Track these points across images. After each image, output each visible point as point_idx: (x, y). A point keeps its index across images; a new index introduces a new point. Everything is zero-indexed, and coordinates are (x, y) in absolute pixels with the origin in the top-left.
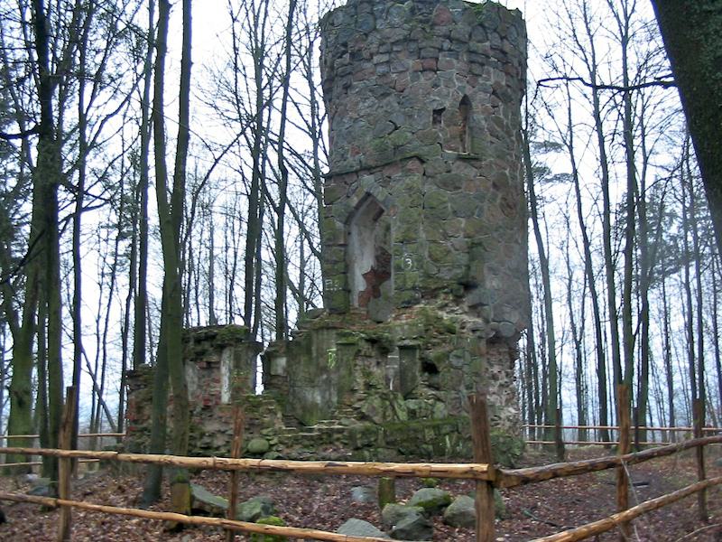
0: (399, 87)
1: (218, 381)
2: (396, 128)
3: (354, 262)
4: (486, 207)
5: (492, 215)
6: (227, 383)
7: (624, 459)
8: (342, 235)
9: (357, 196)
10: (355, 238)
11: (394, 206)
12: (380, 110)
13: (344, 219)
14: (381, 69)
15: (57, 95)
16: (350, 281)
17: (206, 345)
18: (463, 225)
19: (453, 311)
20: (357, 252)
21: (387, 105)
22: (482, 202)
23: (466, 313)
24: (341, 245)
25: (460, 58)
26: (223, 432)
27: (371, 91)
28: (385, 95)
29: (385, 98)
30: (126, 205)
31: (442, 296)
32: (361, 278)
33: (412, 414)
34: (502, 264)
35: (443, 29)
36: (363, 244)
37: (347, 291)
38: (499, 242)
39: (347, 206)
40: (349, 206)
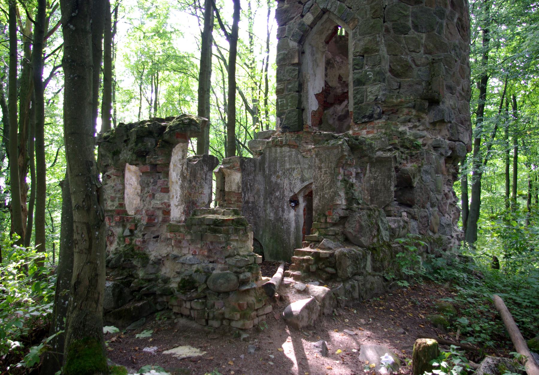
1: (166, 190)
3: (308, 81)
4: (445, 24)
5: (451, 33)
6: (179, 193)
8: (297, 54)
9: (312, 14)
10: (308, 58)
13: (299, 38)
16: (304, 99)
17: (150, 143)
18: (423, 41)
19: (415, 127)
20: (311, 72)
22: (441, 19)
23: (427, 129)
24: (293, 65)
26: (176, 258)
31: (406, 111)
32: (314, 98)
33: (393, 233)
34: (458, 84)
36: (315, 63)
37: (301, 110)
38: (456, 61)
39: (302, 24)
40: (303, 25)
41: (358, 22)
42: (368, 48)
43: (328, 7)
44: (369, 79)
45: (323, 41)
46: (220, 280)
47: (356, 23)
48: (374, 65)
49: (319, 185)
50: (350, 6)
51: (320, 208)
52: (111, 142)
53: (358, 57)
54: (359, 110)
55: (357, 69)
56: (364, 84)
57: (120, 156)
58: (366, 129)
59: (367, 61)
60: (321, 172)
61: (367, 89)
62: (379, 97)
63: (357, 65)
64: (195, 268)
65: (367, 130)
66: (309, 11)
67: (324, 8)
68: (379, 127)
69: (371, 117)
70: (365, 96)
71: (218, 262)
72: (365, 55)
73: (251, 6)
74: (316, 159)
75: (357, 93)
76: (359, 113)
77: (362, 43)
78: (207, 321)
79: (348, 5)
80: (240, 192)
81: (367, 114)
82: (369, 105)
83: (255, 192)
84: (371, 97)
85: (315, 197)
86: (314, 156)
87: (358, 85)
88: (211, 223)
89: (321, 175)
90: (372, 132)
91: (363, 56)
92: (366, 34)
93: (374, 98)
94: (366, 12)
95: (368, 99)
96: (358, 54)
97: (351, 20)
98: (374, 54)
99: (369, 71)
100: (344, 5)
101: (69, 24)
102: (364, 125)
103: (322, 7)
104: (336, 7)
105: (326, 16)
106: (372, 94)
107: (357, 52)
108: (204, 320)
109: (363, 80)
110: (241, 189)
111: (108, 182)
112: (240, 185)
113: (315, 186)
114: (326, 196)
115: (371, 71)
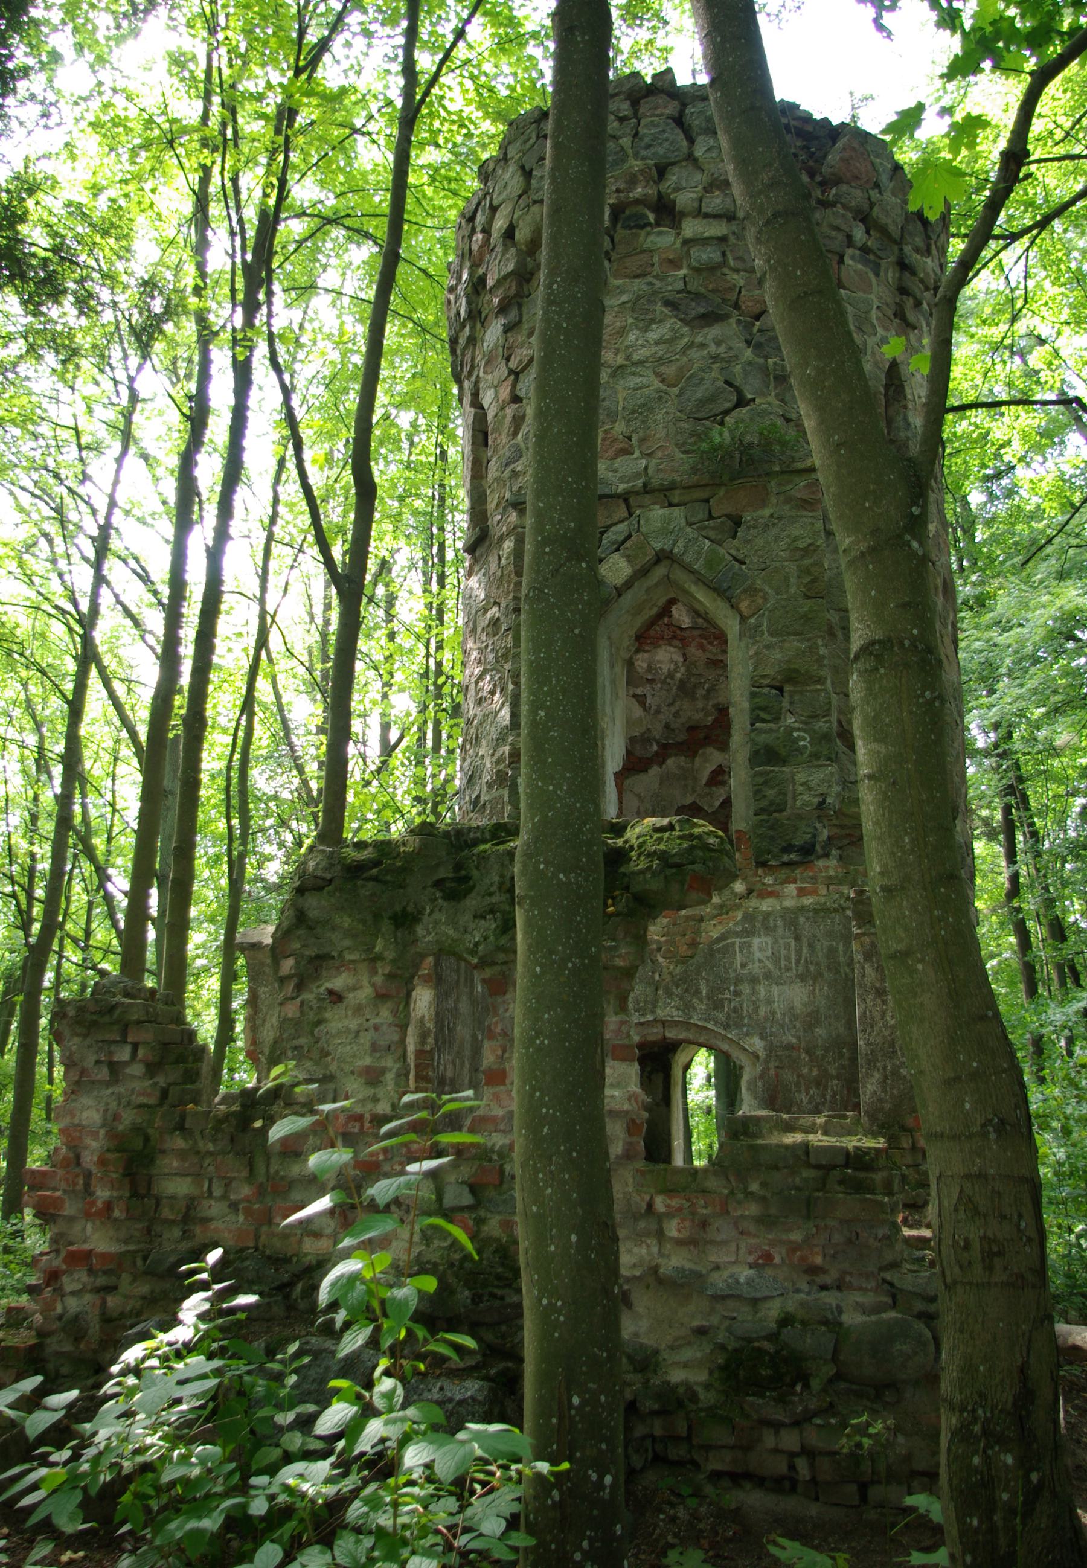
0: (746, 305)
2: (741, 402)
7: (511, 854)
9: (629, 558)
11: (752, 591)
12: (694, 354)
14: (708, 255)
15: (697, 1121)
21: (718, 343)
25: (882, 274)
27: (667, 303)
28: (709, 318)
29: (710, 325)
30: (272, 804)
35: (856, 196)
41: (765, 599)
42: (797, 671)
43: (676, 550)
44: (800, 751)
45: (632, 633)
46: (898, 1346)
47: (760, 601)
48: (815, 717)
49: (879, 1040)
50: (740, 557)
51: (887, 1106)
52: (385, 883)
53: (766, 690)
54: (771, 828)
55: (763, 721)
56: (784, 762)
57: (420, 930)
58: (795, 882)
59: (791, 703)
60: (884, 1002)
61: (793, 774)
62: (829, 800)
63: (763, 709)
64: (773, 1311)
65: (799, 885)
66: (617, 550)
67: (662, 550)
68: (829, 881)
69: (808, 851)
70: (790, 795)
71: (850, 1287)
72: (787, 688)
73: (271, 495)
74: (867, 966)
75: (765, 783)
76: (772, 838)
77: (777, 655)
78: (863, 1488)
79: (733, 552)
80: (428, 1048)
81: (798, 842)
82: (800, 817)
83: (455, 1048)
84: (806, 798)
85: (869, 1075)
86: (858, 957)
87: (768, 762)
88: (841, 1160)
89: (884, 1013)
90: (814, 892)
91: (781, 690)
92: (789, 634)
93: (816, 800)
94: (787, 579)
95: (798, 803)
96: (766, 682)
97: (745, 591)
98: (813, 687)
99: (798, 730)
100: (722, 551)
101: (908, 537)
102: (784, 872)
103: (658, 546)
104: (699, 553)
105: (660, 571)
106: (810, 789)
107: (764, 677)
108: (853, 1488)
109: (783, 752)
110: (430, 1040)
111: (328, 1015)
112: (430, 1025)
113: (867, 1044)
114: (903, 1071)
115: (805, 731)
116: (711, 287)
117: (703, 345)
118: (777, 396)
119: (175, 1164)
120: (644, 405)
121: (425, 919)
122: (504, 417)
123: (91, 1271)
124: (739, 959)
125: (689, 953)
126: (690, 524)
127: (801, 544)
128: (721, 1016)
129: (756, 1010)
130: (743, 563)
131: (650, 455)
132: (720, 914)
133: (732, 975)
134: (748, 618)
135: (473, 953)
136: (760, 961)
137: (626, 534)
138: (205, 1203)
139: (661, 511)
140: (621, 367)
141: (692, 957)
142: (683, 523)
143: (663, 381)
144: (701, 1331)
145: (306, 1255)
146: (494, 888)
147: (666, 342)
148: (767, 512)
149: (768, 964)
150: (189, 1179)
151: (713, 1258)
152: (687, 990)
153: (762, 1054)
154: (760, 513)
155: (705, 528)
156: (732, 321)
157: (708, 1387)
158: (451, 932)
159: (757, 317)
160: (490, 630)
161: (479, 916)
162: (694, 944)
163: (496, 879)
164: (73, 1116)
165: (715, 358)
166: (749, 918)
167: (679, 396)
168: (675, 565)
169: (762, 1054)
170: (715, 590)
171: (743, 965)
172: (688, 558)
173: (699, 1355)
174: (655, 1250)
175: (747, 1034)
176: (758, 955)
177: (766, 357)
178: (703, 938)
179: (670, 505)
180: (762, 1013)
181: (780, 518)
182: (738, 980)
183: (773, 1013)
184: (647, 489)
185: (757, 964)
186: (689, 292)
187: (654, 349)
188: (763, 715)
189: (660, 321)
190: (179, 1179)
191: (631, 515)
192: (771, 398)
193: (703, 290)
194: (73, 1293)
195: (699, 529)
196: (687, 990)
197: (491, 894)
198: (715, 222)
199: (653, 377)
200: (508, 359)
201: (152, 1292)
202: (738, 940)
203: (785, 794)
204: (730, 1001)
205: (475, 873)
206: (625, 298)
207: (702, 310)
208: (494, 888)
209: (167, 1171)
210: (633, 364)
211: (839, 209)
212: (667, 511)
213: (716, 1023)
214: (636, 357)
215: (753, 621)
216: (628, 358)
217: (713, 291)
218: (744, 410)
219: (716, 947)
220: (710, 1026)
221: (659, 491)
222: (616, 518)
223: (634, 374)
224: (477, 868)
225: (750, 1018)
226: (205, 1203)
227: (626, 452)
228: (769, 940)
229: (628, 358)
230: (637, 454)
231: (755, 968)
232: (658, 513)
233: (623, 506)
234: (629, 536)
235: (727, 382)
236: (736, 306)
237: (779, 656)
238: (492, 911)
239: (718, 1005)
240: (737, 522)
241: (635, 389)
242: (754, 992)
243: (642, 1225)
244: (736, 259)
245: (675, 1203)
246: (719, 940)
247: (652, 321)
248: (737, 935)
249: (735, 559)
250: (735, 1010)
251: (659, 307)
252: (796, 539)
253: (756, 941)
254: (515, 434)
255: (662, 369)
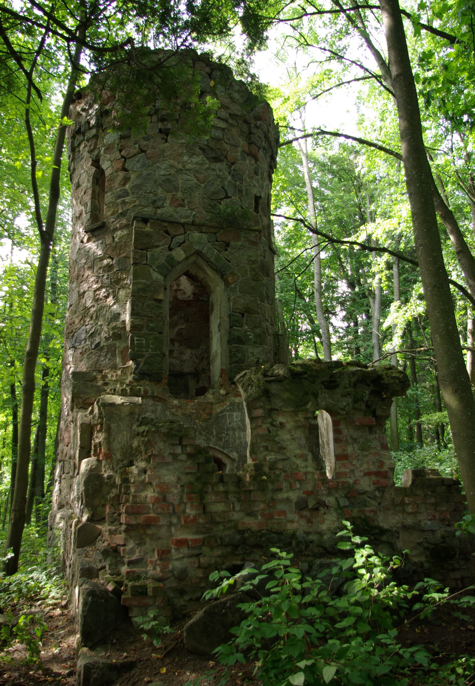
2: (227, 197)
9: (184, 251)
11: (233, 274)
27: (201, 148)
28: (216, 159)
41: (238, 278)
43: (203, 251)
44: (250, 340)
48: (255, 327)
50: (229, 259)
53: (237, 314)
55: (236, 326)
56: (244, 343)
64: (439, 534)
66: (179, 246)
72: (245, 314)
79: (226, 256)
84: (252, 358)
88: (452, 483)
91: (243, 315)
93: (256, 360)
95: (249, 360)
96: (238, 311)
97: (230, 273)
99: (249, 331)
106: (254, 355)
107: (237, 309)
116: (218, 147)
117: (214, 170)
118: (239, 197)
119: (213, 498)
120: (190, 188)
121: (320, 395)
122: (118, 176)
123: (188, 547)
124: (228, 421)
125: (208, 417)
126: (209, 242)
127: (252, 259)
128: (222, 444)
129: (235, 441)
130: (229, 262)
131: (192, 209)
132: (219, 403)
133: (225, 427)
134: (230, 284)
135: (343, 409)
136: (236, 422)
137: (183, 240)
138: (230, 514)
139: (198, 234)
140: (181, 169)
141: (210, 419)
142: (207, 241)
143: (198, 180)
144: (419, 544)
145: (288, 530)
146: (347, 386)
147: (199, 164)
148: (240, 243)
149: (240, 423)
150: (223, 504)
151: (419, 518)
152: (208, 433)
153: (237, 459)
154: (237, 243)
155: (215, 244)
156: (225, 163)
157: (426, 562)
158: (331, 401)
159: (233, 164)
160: (106, 269)
161: (344, 396)
162: (210, 414)
163: (347, 382)
164: (160, 479)
165: (218, 176)
166: (232, 404)
167: (205, 188)
168: (199, 257)
169: (237, 459)
170: (215, 270)
171: (230, 423)
172: (209, 255)
173: (418, 552)
174: (401, 517)
175: (231, 451)
176: (235, 419)
177: (236, 181)
178: (214, 412)
179: (201, 232)
180: (237, 443)
181: (245, 247)
182: (228, 429)
183: (241, 443)
184: (193, 224)
185: (235, 423)
186: (209, 147)
187: (195, 166)
188: (237, 324)
189: (197, 155)
190: (218, 504)
191: (185, 233)
192: (237, 198)
193: (214, 147)
194: (177, 560)
195: (213, 244)
196: (208, 433)
197: (347, 388)
198: (222, 122)
199: (194, 178)
200: (120, 151)
201: (223, 553)
202: (228, 413)
203: (245, 356)
204: (225, 437)
205: (338, 380)
206: (183, 141)
207: (214, 155)
208: (347, 386)
209: (210, 501)
210: (186, 170)
211: (260, 130)
212: (201, 234)
213: (219, 446)
214: (187, 167)
215: (233, 286)
216: (184, 166)
217: (218, 149)
218: (228, 200)
219: (219, 415)
220: (217, 447)
221: (197, 225)
222: (179, 233)
223: (186, 174)
224: (339, 377)
225: (232, 444)
226: (230, 514)
227: (183, 206)
228: (240, 414)
229: (184, 166)
230: (186, 208)
231: (234, 425)
232: (196, 235)
233: (182, 228)
234: (184, 242)
235: (222, 187)
236: (226, 157)
237: (243, 301)
238: (349, 394)
239: (220, 439)
240: (228, 245)
241: (186, 180)
242: (234, 434)
243: (398, 508)
244: (227, 138)
245: (411, 500)
246: (220, 413)
247: (194, 154)
248: (228, 411)
249: (226, 259)
250: (227, 441)
251: (197, 149)
252: (250, 256)
253: (235, 414)
254: (124, 184)
255: (197, 175)
